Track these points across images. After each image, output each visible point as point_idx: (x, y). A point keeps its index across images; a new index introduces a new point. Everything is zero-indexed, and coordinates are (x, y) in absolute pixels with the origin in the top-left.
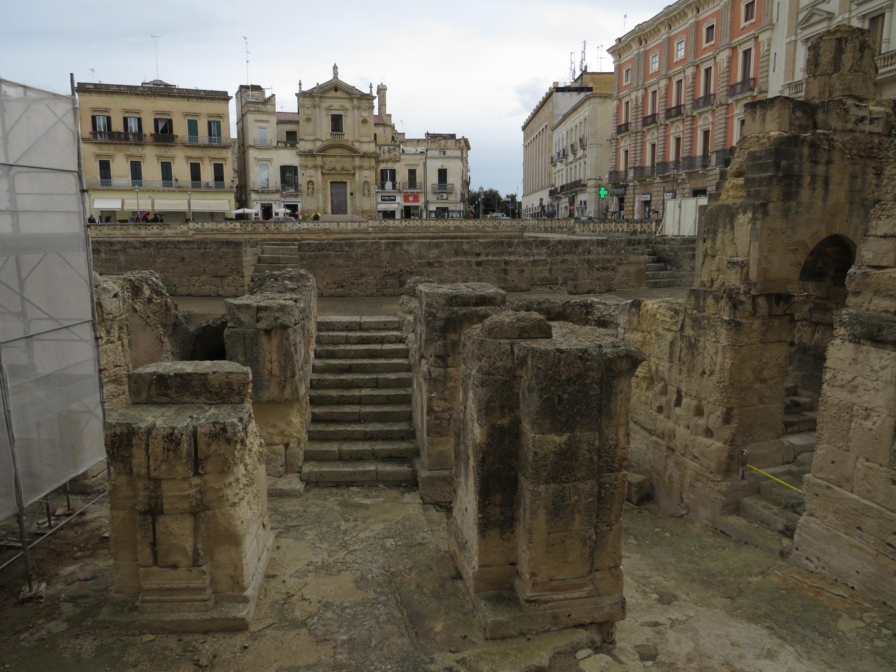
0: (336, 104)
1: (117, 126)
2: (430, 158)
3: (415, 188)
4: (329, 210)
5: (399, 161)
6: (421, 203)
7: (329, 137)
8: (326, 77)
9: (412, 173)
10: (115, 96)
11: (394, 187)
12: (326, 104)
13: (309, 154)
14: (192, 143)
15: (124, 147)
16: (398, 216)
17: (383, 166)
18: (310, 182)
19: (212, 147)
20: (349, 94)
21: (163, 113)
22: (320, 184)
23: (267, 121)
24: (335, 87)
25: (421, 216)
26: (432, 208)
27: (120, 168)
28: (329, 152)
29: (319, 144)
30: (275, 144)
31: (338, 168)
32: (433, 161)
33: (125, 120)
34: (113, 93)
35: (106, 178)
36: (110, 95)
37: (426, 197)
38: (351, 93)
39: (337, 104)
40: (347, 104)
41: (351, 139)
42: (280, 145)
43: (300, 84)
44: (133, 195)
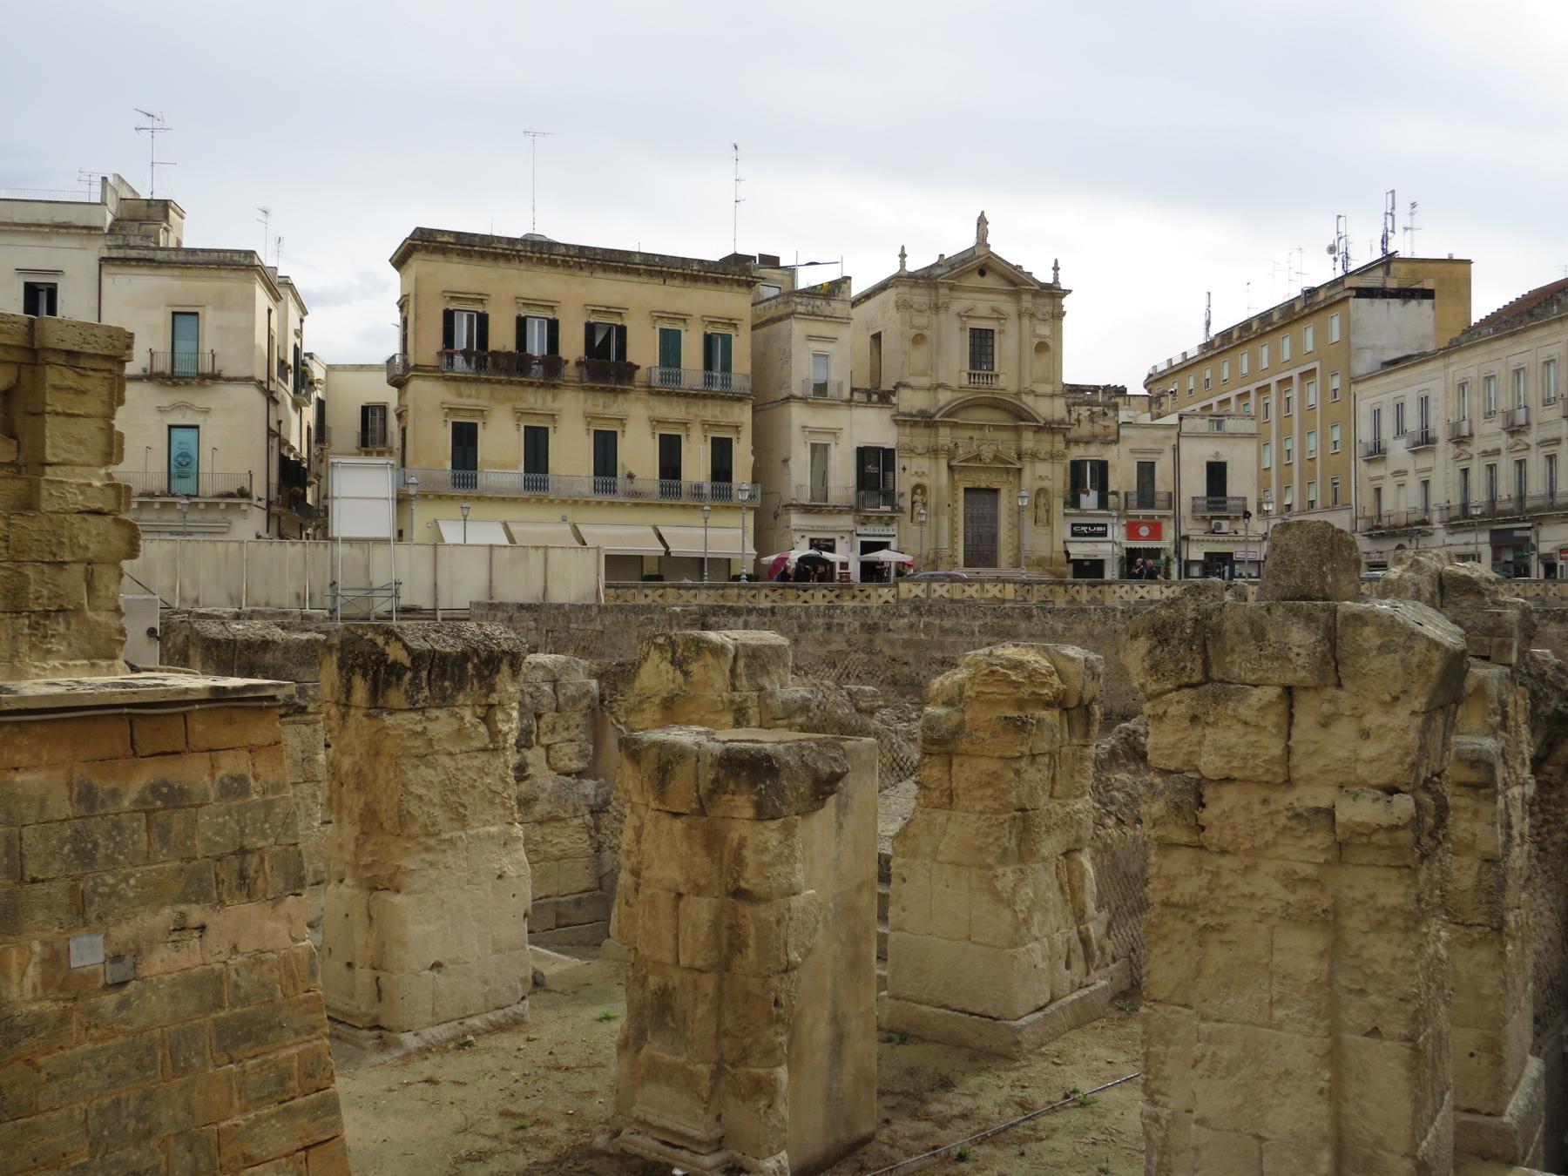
0: (983, 304)
1: (502, 338)
2: (1191, 435)
3: (1152, 506)
4: (961, 559)
5: (1116, 441)
6: (1167, 542)
8: (960, 241)
9: (1146, 471)
10: (502, 264)
11: (1103, 503)
12: (961, 303)
13: (925, 420)
14: (668, 387)
15: (513, 391)
16: (1111, 572)
17: (1077, 453)
18: (919, 488)
19: (714, 397)
20: (1011, 282)
21: (609, 311)
22: (945, 493)
23: (832, 340)
24: (979, 265)
25: (1167, 575)
26: (1196, 553)
27: (500, 443)
29: (944, 397)
30: (846, 394)
31: (987, 452)
32: (1195, 442)
33: (521, 323)
34: (496, 257)
35: (605, 474)
36: (489, 262)
37: (1177, 529)
38: (1015, 281)
39: (982, 304)
40: (1007, 306)
42: (856, 395)
43: (903, 256)
44: (454, 510)
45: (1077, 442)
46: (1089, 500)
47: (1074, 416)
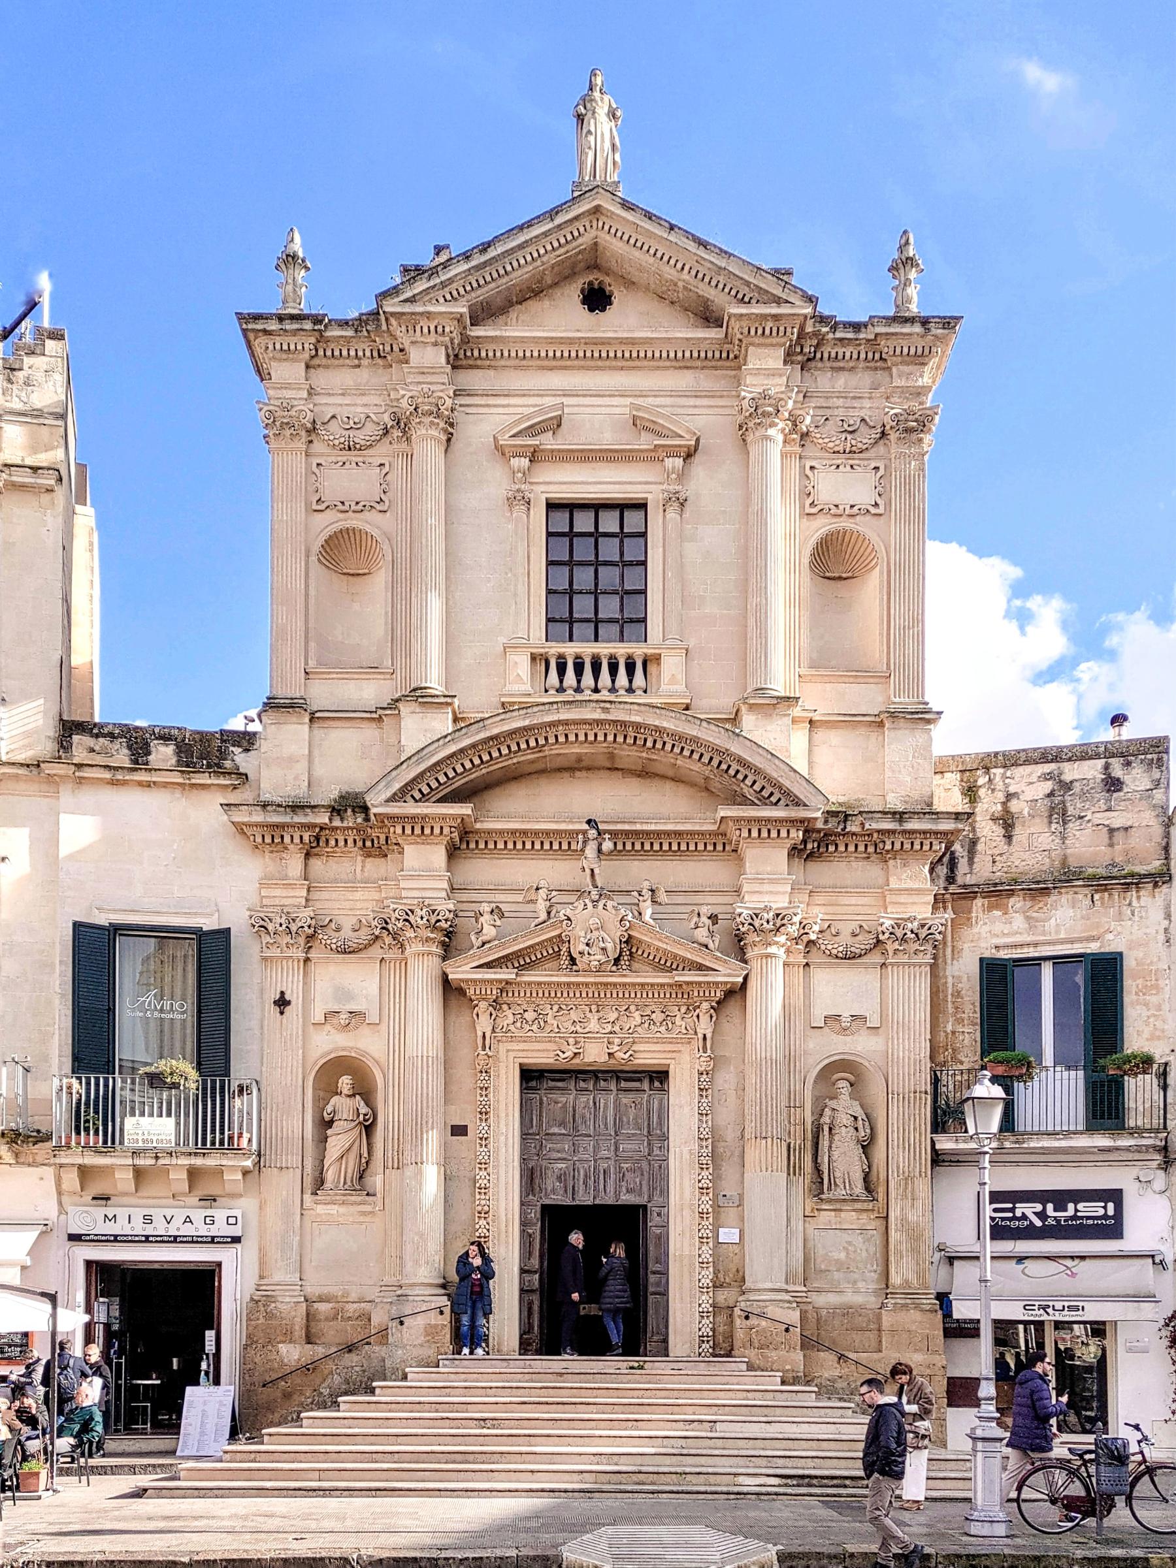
0: (597, 406)
7: (520, 678)
11: (1105, 1107)
12: (502, 407)
13: (346, 823)
17: (997, 932)
28: (509, 811)
29: (421, 731)
31: (593, 927)
40: (688, 404)
41: (717, 698)
45: (997, 892)
46: (1055, 1093)
47: (989, 804)
